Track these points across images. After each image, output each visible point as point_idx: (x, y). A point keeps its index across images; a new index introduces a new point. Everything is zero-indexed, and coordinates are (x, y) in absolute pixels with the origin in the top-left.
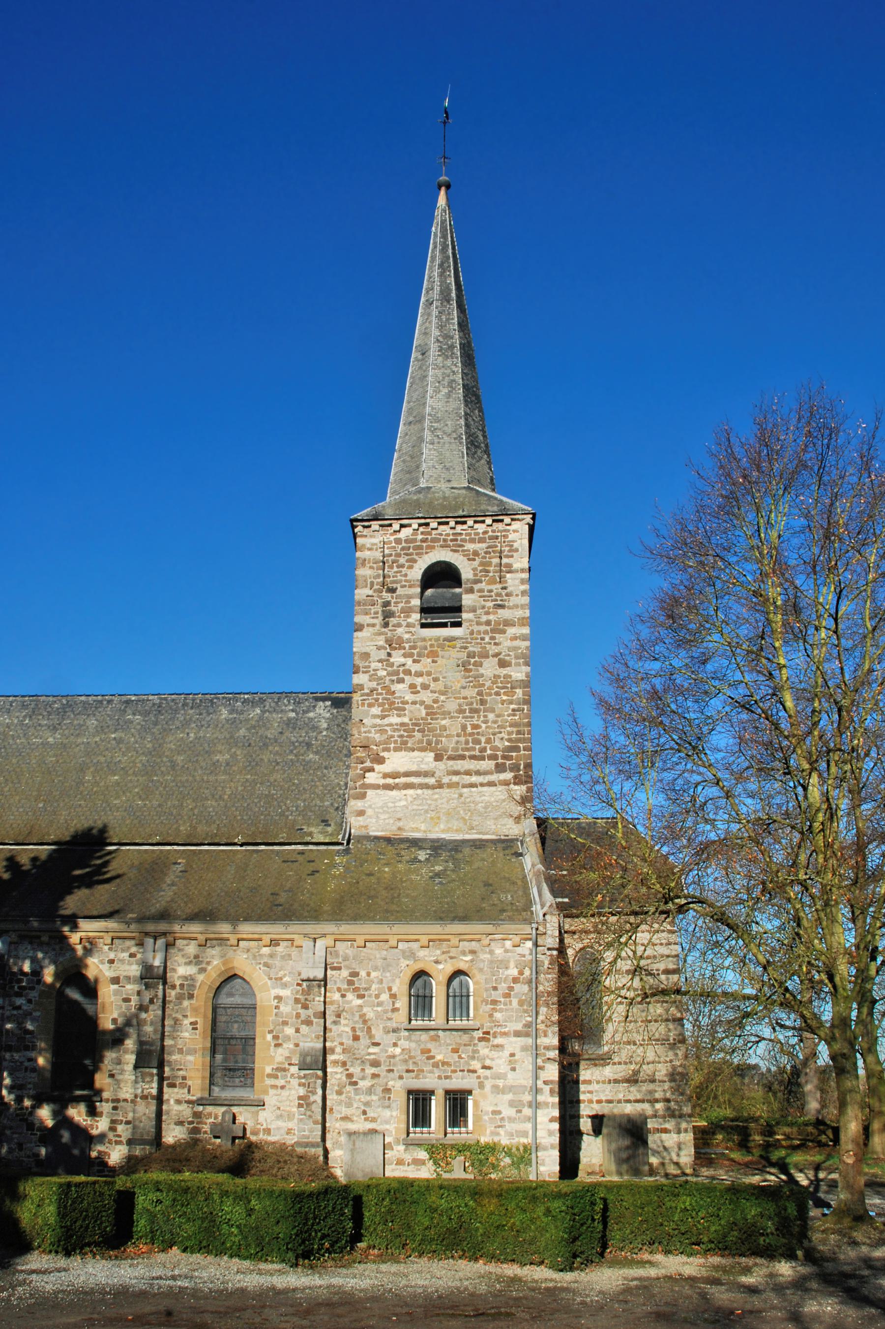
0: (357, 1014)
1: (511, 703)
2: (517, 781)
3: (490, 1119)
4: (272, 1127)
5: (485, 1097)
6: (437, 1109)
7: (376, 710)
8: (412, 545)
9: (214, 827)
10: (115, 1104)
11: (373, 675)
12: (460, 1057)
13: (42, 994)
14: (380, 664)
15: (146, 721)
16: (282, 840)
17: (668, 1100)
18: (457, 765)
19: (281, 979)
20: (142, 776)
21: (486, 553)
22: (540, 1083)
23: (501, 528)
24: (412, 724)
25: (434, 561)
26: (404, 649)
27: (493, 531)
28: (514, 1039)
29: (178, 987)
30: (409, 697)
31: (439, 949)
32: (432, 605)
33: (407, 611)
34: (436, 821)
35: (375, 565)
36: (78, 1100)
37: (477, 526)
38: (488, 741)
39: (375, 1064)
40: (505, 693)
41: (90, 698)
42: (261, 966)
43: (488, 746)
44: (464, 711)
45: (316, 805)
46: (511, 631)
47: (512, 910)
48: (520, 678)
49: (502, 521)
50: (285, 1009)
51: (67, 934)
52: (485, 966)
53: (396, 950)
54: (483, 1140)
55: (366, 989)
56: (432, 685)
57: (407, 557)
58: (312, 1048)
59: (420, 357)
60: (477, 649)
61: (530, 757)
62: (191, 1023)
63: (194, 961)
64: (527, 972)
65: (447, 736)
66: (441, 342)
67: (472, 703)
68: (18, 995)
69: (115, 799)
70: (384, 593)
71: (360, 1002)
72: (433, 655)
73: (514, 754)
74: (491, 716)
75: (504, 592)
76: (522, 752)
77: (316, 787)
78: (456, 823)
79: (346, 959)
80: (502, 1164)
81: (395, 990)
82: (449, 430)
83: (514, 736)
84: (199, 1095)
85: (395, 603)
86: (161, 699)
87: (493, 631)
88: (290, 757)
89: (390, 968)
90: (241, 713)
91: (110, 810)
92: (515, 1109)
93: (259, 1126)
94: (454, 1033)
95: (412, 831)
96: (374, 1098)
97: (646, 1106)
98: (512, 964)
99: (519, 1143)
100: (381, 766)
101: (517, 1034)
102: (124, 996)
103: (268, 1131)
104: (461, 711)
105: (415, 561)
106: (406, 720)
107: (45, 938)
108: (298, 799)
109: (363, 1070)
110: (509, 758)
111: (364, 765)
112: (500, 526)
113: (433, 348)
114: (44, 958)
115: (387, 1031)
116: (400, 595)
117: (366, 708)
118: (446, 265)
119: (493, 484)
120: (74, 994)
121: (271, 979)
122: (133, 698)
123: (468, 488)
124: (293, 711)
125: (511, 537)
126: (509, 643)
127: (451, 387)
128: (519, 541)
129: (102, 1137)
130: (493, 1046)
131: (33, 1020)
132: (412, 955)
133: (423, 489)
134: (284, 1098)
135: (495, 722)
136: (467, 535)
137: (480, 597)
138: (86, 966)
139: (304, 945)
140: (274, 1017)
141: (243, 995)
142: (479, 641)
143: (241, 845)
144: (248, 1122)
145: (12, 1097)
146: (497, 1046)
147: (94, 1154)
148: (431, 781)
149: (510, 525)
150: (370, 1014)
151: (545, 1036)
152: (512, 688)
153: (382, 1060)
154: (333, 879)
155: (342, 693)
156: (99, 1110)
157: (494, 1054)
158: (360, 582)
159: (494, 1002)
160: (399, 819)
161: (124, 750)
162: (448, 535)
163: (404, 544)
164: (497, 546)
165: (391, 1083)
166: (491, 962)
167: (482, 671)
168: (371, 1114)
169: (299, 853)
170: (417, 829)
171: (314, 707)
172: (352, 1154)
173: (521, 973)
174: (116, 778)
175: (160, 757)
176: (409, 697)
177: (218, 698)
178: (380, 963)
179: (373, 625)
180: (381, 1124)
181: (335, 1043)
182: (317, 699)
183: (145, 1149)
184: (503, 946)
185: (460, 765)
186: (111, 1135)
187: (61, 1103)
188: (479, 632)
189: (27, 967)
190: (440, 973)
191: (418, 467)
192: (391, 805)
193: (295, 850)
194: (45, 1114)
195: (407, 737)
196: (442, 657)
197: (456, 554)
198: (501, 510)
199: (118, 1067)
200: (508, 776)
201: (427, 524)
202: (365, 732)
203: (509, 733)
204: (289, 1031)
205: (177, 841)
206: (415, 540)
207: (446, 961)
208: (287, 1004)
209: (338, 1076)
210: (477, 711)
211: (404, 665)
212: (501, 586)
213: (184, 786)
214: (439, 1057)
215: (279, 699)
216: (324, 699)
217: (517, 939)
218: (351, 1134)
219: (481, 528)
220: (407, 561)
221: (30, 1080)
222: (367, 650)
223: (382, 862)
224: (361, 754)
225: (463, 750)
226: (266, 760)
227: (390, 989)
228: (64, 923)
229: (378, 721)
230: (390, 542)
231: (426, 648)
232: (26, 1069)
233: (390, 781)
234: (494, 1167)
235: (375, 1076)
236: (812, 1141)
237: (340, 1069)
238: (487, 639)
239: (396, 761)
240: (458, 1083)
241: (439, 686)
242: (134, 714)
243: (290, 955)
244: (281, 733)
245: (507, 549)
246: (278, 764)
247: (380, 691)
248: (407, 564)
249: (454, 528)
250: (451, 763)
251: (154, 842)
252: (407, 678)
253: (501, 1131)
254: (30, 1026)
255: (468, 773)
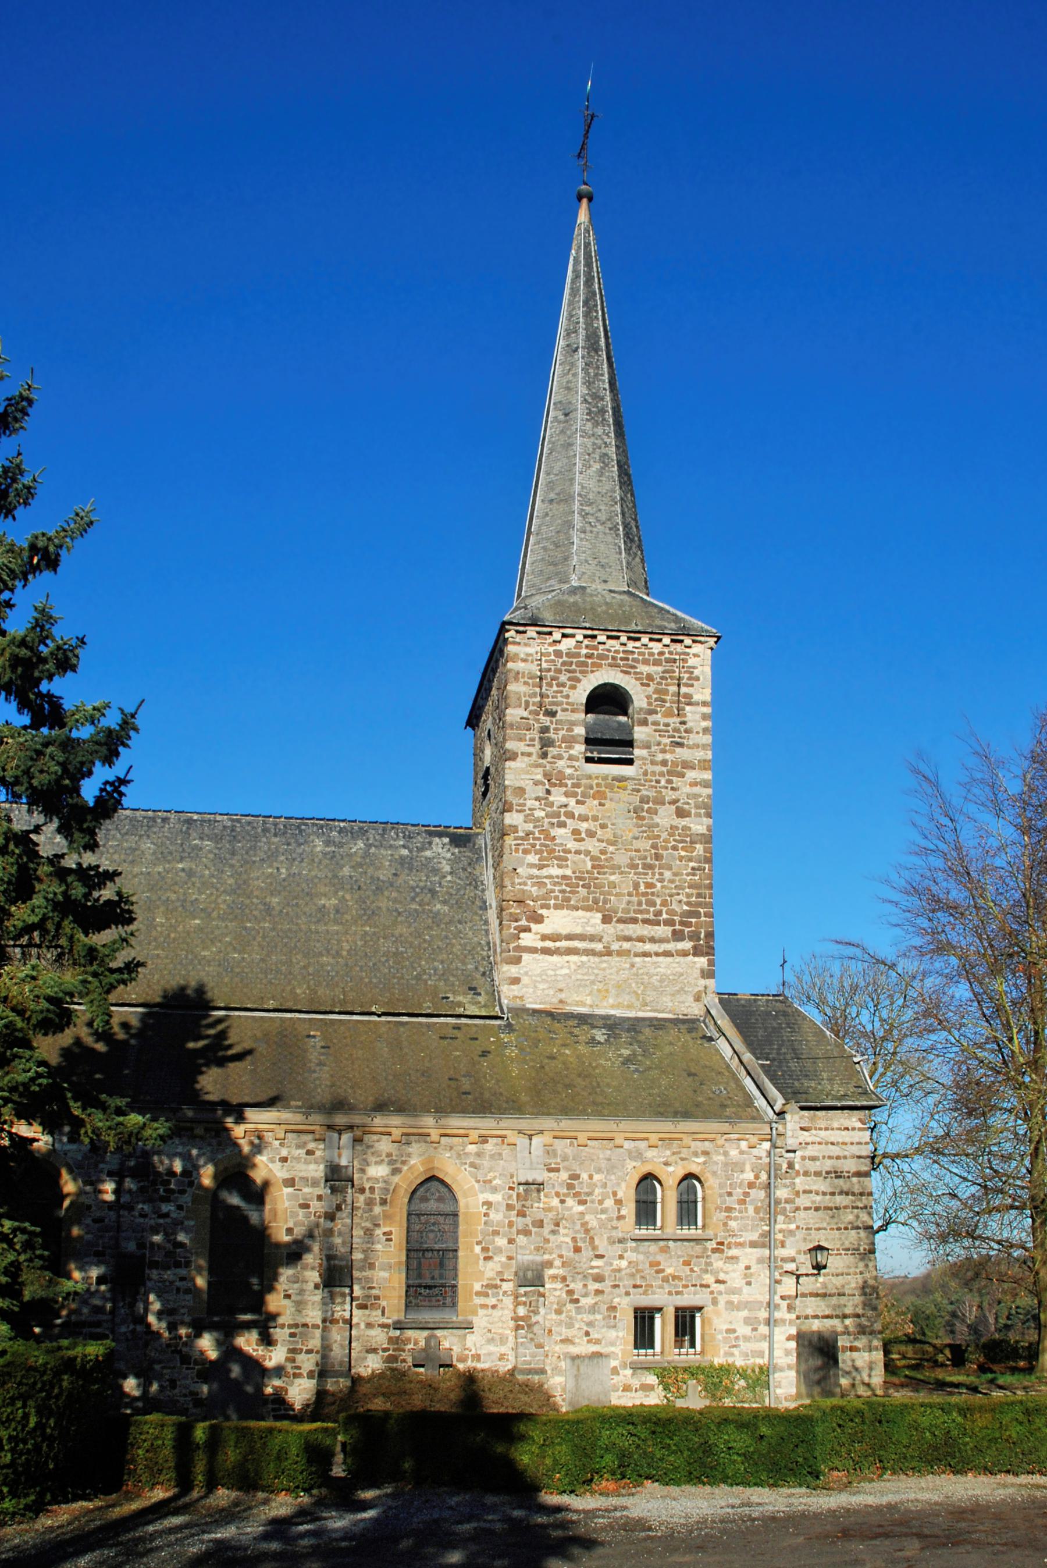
0: (579, 1223)
1: (690, 860)
2: (697, 952)
3: (724, 1338)
4: (482, 1352)
5: (718, 1314)
6: (663, 1328)
7: (533, 859)
8: (575, 660)
9: (337, 991)
10: (292, 1331)
11: (529, 815)
12: (692, 1270)
13: (196, 1199)
14: (537, 803)
15: (220, 849)
16: (429, 1011)
17: (858, 1316)
18: (628, 929)
19: (490, 1181)
20: (231, 921)
21: (662, 678)
22: (777, 1299)
23: (679, 650)
24: (577, 878)
25: (601, 682)
26: (566, 786)
27: (671, 653)
28: (749, 1250)
29: (367, 1191)
30: (572, 845)
31: (669, 1149)
32: (599, 736)
33: (570, 741)
34: (604, 993)
35: (530, 681)
36: (248, 1326)
37: (651, 644)
38: (664, 903)
39: (599, 1278)
40: (683, 848)
41: (138, 813)
42: (467, 1166)
43: (664, 909)
44: (636, 866)
45: (457, 969)
46: (691, 775)
47: (734, 1106)
48: (701, 832)
49: (682, 641)
50: (496, 1216)
51: (230, 1125)
52: (718, 1169)
53: (621, 1150)
54: (717, 1361)
55: (589, 1194)
56: (599, 832)
57: (569, 675)
58: (533, 1262)
59: (562, 417)
60: (652, 794)
61: (712, 924)
62: (384, 1234)
63: (386, 1159)
64: (764, 1176)
65: (616, 895)
66: (589, 403)
67: (645, 858)
68: (166, 1200)
69: (203, 949)
70: (541, 716)
71: (581, 1208)
72: (600, 796)
73: (693, 920)
74: (668, 874)
75: (682, 728)
76: (703, 919)
77: (453, 945)
78: (627, 997)
79: (565, 1159)
80: (737, 1387)
81: (620, 1195)
82: (603, 517)
83: (694, 899)
84: (395, 1318)
85: (556, 729)
86: (233, 820)
87: (669, 773)
88: (414, 906)
89: (615, 1170)
90: (341, 845)
91: (200, 964)
92: (750, 1328)
93: (467, 1352)
94: (685, 1243)
95: (577, 1005)
96: (599, 1317)
97: (836, 1322)
98: (748, 1167)
99: (754, 1364)
100: (539, 926)
101: (753, 1245)
102: (301, 1202)
103: (477, 1357)
104: (633, 866)
105: (579, 681)
106: (568, 872)
107: (199, 1131)
108: (434, 960)
109: (585, 1286)
110: (689, 925)
111: (520, 923)
112: (678, 647)
113: (581, 410)
114: (199, 1156)
115: (612, 1242)
116: (561, 720)
117: (520, 854)
118: (592, 303)
119: (647, 588)
120: (235, 1200)
121: (478, 1181)
122: (195, 817)
123: (628, 593)
124: (404, 847)
125: (692, 662)
126: (687, 789)
127: (603, 462)
128: (700, 668)
129: (279, 1371)
130: (728, 1258)
131: (187, 1231)
132: (638, 1155)
133: (576, 588)
134: (496, 1319)
135: (672, 881)
136: (640, 654)
137: (655, 731)
138: (254, 1166)
139: (518, 1143)
140: (483, 1226)
141: (441, 1199)
142: (653, 783)
143: (379, 1016)
144: (454, 1348)
145: (164, 1325)
146: (732, 1258)
147: (269, 1390)
148: (599, 947)
149: (689, 647)
150: (592, 1221)
151: (783, 1246)
152: (692, 842)
153: (606, 1274)
154: (512, 1062)
155: (461, 828)
156: (276, 1337)
157: (728, 1267)
158: (512, 700)
159: (729, 1209)
160: (561, 990)
161: (198, 885)
162: (617, 652)
163: (565, 659)
164: (674, 672)
165: (616, 1300)
166: (726, 1164)
167: (657, 819)
168: (594, 1335)
169: (454, 1028)
170: (581, 1002)
171: (430, 843)
172: (577, 1380)
173: (757, 1177)
174: (197, 922)
175: (249, 897)
176: (572, 845)
177: (306, 825)
178: (603, 1164)
179: (529, 755)
180: (606, 1346)
181: (554, 1256)
182: (431, 834)
183: (338, 1382)
184: (738, 1147)
185: (631, 930)
186: (289, 1367)
187: (228, 1330)
188: (654, 773)
189: (178, 1166)
190: (671, 1174)
191: (566, 559)
192: (551, 973)
193: (447, 1024)
194: (207, 1345)
195: (570, 892)
196: (611, 800)
197: (627, 677)
198: (680, 629)
199: (296, 1286)
200: (687, 945)
201: (594, 637)
202: (520, 884)
203: (688, 896)
204: (501, 1242)
205: (299, 1007)
206: (578, 655)
207: (676, 1163)
208: (497, 1211)
209: (558, 1293)
210: (651, 867)
211: (566, 806)
212: (679, 720)
213: (287, 937)
214: (669, 1271)
215: (384, 830)
216: (440, 835)
217: (754, 1140)
218: (574, 1358)
219: (656, 647)
220: (569, 679)
221: (183, 1303)
222: (522, 784)
223: (558, 1042)
224: (515, 910)
225: (635, 912)
226: (384, 909)
227: (615, 1194)
228: (227, 1113)
229: (535, 872)
230: (549, 654)
231: (591, 788)
232: (178, 1290)
233: (549, 944)
234: (729, 1391)
235: (598, 1292)
236: (927, 1360)
237: (559, 1285)
238: (663, 783)
239: (558, 921)
240: (687, 1299)
241: (608, 834)
242: (201, 839)
243: (500, 1154)
244: (395, 875)
245: (687, 676)
246: (399, 914)
247: (537, 835)
248: (569, 683)
249: (625, 645)
250: (621, 926)
251: (271, 1007)
252: (569, 821)
253: (735, 1351)
254: (182, 1237)
255: (641, 939)
